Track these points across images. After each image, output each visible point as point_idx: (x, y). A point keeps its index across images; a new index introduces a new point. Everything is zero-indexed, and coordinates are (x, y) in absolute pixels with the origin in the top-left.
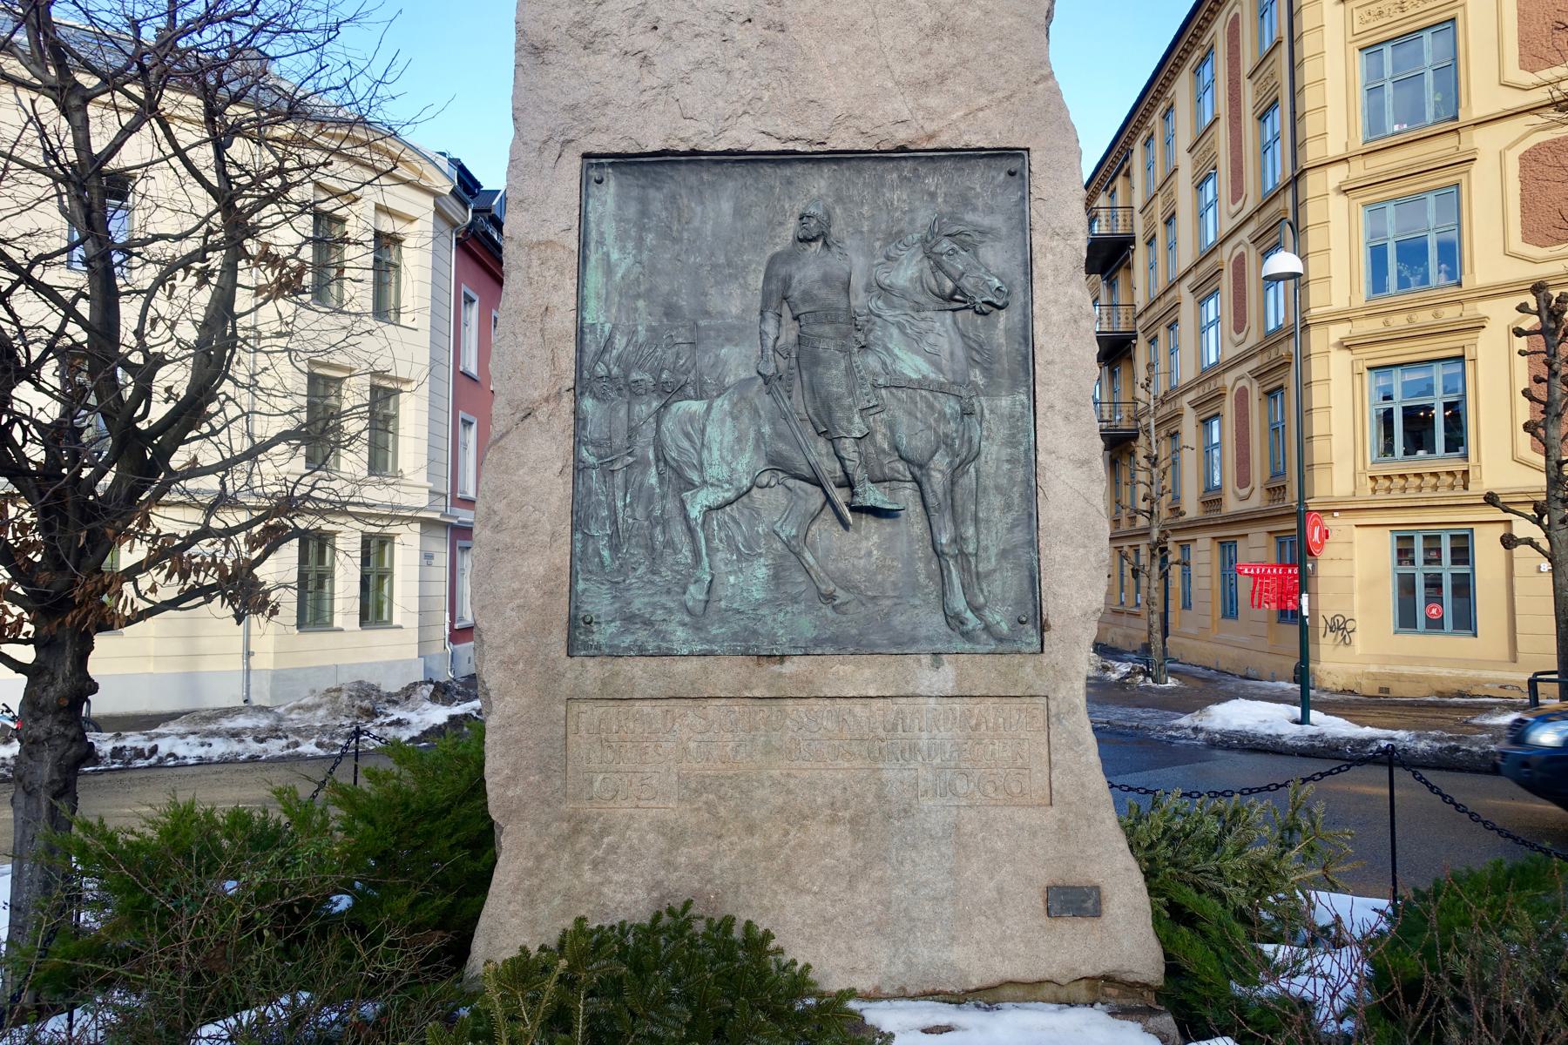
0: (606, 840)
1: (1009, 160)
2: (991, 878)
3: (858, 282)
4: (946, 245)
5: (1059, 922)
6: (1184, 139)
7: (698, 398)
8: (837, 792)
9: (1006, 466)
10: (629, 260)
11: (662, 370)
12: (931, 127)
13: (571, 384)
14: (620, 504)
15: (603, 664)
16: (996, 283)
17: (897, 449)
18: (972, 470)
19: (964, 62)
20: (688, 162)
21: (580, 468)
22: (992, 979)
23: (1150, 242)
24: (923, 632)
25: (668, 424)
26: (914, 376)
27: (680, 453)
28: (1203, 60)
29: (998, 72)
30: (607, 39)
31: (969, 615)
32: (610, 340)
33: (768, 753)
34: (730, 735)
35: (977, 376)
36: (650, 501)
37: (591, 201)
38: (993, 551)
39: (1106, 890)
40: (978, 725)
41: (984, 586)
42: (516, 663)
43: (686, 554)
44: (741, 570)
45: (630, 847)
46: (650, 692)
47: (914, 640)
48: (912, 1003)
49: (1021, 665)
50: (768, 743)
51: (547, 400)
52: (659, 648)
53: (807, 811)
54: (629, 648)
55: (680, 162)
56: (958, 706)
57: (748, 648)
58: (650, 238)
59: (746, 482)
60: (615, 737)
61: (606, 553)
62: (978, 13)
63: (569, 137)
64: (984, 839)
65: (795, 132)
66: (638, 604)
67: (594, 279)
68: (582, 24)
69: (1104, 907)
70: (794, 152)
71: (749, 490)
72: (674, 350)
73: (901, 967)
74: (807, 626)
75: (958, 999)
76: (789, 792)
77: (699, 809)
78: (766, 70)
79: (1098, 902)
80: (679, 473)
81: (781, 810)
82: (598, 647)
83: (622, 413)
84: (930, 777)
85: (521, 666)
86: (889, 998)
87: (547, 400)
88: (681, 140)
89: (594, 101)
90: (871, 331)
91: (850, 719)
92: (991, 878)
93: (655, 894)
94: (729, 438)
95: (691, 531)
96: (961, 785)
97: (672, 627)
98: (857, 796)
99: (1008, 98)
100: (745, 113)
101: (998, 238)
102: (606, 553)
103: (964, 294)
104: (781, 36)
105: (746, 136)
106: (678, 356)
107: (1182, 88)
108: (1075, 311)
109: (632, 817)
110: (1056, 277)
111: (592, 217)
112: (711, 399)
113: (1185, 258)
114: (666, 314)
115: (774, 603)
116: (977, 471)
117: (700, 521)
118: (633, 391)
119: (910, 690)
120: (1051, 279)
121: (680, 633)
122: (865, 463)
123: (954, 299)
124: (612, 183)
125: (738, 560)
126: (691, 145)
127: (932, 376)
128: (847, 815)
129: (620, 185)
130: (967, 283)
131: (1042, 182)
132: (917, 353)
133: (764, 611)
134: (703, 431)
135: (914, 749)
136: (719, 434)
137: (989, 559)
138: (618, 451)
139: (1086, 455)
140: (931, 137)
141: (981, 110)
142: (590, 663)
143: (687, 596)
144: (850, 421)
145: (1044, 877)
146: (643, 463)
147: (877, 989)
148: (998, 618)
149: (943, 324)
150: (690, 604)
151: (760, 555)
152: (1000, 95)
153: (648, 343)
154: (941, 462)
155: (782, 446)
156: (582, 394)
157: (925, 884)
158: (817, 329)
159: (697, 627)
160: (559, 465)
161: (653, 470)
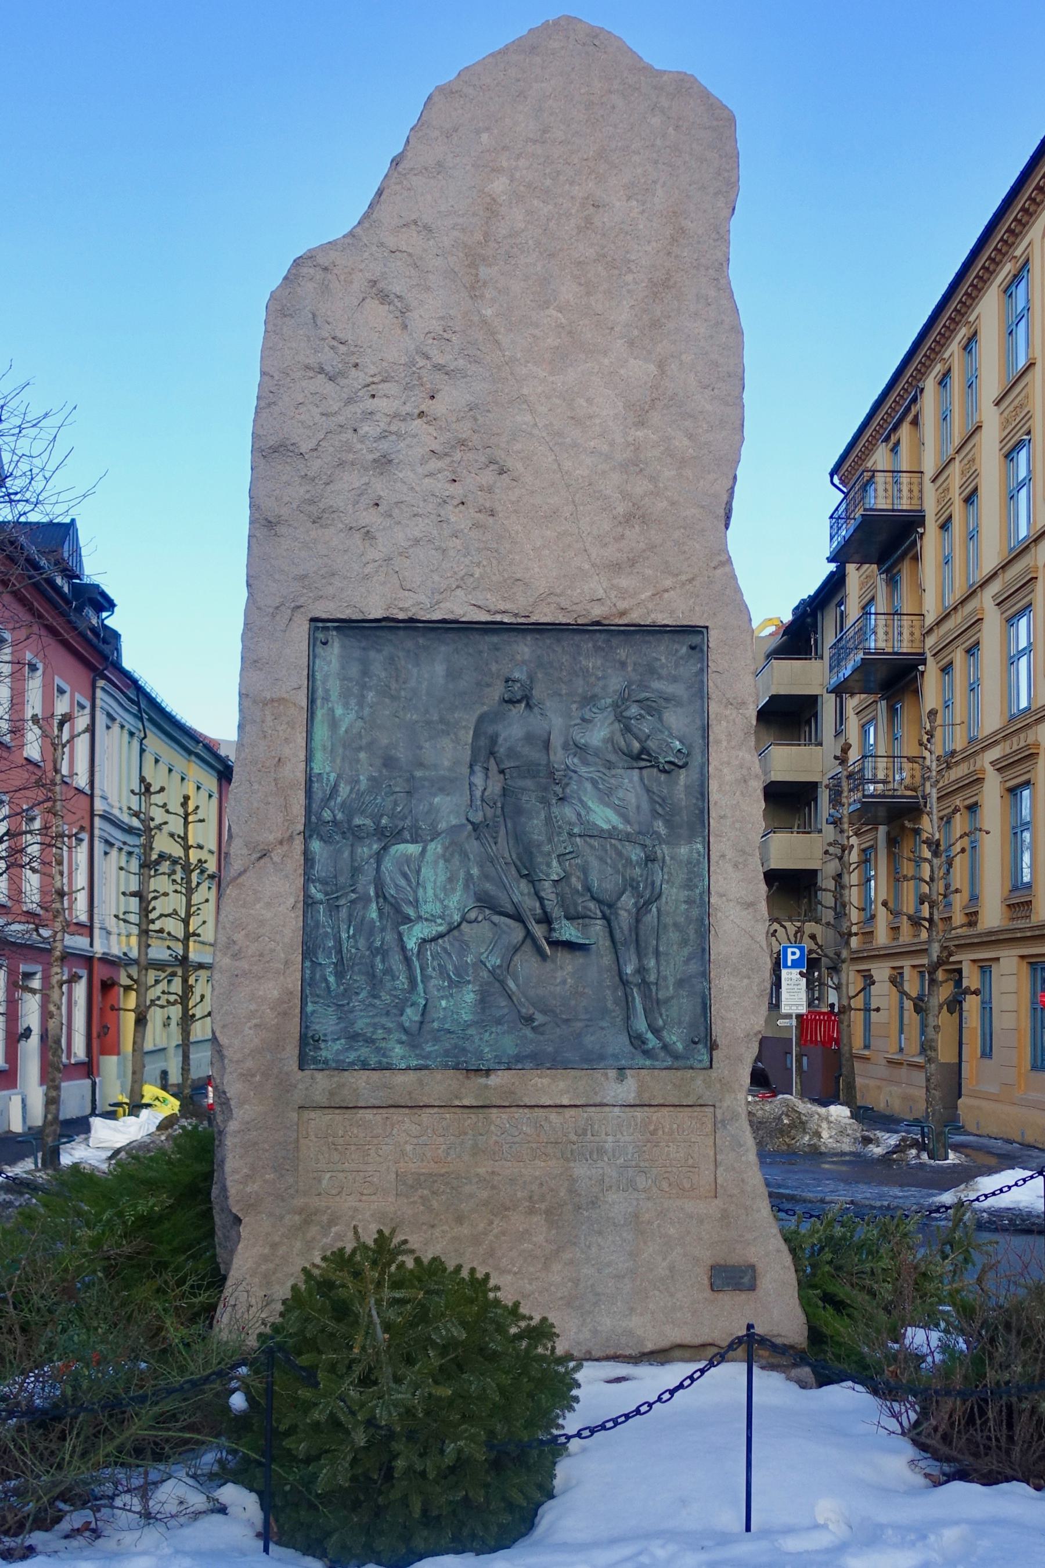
0: (333, 1230)
1: (691, 636)
2: (664, 1259)
3: (557, 741)
4: (634, 710)
6: (990, 386)
7: (414, 841)
8: (535, 1187)
9: (684, 906)
10: (352, 716)
11: (382, 816)
12: (622, 605)
14: (344, 936)
16: (677, 745)
18: (654, 909)
19: (652, 547)
20: (405, 628)
21: (309, 903)
23: (945, 526)
25: (387, 864)
26: (605, 826)
28: (1016, 278)
30: (335, 516)
31: (650, 1035)
33: (474, 1154)
35: (660, 827)
38: (671, 981)
39: (760, 1267)
40: (656, 1130)
41: (663, 1011)
42: (253, 1076)
43: (402, 981)
44: (451, 995)
46: (373, 1102)
47: (602, 1057)
49: (693, 1079)
51: (281, 843)
52: (380, 1062)
54: (353, 1063)
56: (639, 1114)
58: (371, 696)
60: (341, 1141)
61: (332, 979)
64: (659, 1226)
65: (502, 606)
66: (360, 1025)
68: (312, 502)
70: (502, 623)
71: (459, 925)
72: (392, 798)
73: (588, 1335)
74: (509, 1045)
77: (414, 1203)
79: (754, 1278)
80: (398, 910)
87: (281, 843)
88: (401, 609)
90: (568, 784)
91: (546, 1126)
94: (442, 878)
95: (407, 961)
98: (552, 1190)
100: (458, 587)
102: (332, 979)
105: (460, 607)
107: (989, 309)
108: (745, 772)
113: (990, 559)
114: (385, 765)
116: (659, 910)
117: (415, 951)
118: (356, 835)
120: (724, 744)
121: (399, 1050)
122: (562, 903)
123: (641, 757)
125: (450, 987)
126: (410, 614)
127: (621, 826)
128: (543, 1207)
129: (343, 647)
131: (718, 657)
132: (607, 805)
135: (601, 1151)
136: (433, 875)
137: (668, 988)
139: (751, 899)
140: (622, 614)
142: (319, 1076)
148: (674, 1038)
149: (631, 781)
150: (407, 1024)
152: (684, 578)
154: (627, 901)
156: (311, 836)
157: (609, 1264)
158: (521, 783)
161: (374, 906)
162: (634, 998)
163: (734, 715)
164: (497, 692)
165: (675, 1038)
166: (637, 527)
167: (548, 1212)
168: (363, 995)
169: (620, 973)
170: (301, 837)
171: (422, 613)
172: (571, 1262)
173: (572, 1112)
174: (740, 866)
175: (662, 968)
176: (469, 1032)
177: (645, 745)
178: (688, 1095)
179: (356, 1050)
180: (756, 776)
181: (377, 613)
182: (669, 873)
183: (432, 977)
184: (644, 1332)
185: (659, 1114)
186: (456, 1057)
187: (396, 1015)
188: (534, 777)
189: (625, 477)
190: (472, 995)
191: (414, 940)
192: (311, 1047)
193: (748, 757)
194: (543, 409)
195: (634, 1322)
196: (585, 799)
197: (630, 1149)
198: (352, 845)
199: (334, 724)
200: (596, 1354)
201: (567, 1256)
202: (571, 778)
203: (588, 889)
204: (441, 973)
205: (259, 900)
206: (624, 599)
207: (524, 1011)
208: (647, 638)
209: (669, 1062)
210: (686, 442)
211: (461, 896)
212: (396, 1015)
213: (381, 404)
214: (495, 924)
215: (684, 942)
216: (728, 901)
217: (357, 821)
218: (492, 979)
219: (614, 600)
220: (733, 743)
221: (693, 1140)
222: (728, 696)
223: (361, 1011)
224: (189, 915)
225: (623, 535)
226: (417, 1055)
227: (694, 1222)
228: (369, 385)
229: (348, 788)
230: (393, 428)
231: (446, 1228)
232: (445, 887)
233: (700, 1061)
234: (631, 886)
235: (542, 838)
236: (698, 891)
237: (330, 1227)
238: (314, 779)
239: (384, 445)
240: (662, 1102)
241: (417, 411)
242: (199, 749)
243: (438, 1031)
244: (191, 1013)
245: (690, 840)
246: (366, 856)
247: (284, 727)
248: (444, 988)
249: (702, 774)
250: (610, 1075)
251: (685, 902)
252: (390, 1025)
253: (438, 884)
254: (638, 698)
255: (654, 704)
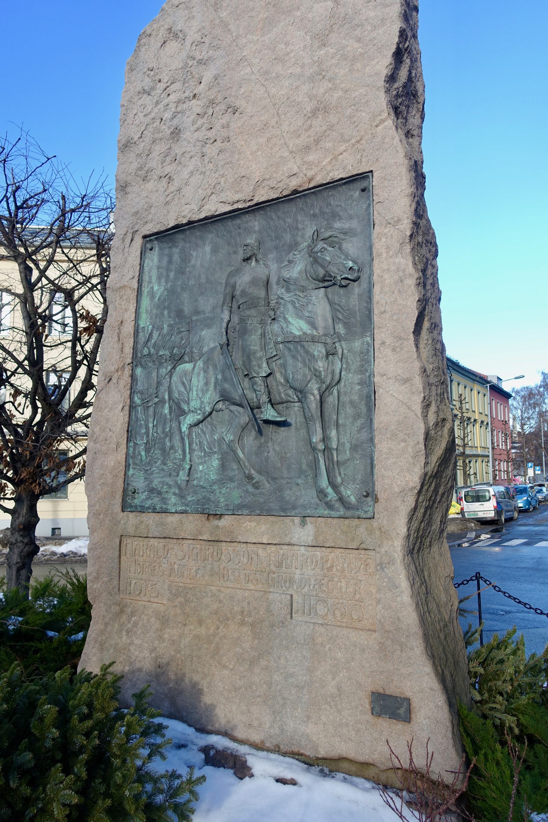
0: (133, 619)
2: (333, 679)
4: (321, 245)
5: (380, 721)
8: (245, 604)
9: (358, 387)
10: (162, 289)
11: (174, 348)
12: (310, 174)
13: (129, 361)
14: (151, 425)
15: (137, 516)
16: (350, 264)
17: (288, 382)
18: (335, 392)
19: (331, 127)
20: (189, 228)
21: (132, 407)
22: (334, 753)
24: (301, 501)
26: (297, 333)
27: (179, 394)
29: (352, 126)
30: (152, 173)
31: (330, 490)
32: (151, 335)
33: (212, 575)
34: (193, 562)
35: (341, 329)
36: (165, 424)
37: (146, 261)
38: (348, 445)
39: (415, 703)
40: (332, 567)
41: (342, 470)
42: (100, 514)
43: (179, 454)
44: (205, 462)
45: (143, 625)
46: (157, 534)
47: (294, 507)
48: (281, 758)
49: (357, 527)
50: (212, 569)
52: (161, 508)
53: (229, 615)
54: (149, 508)
55: (185, 230)
56: (318, 553)
57: (204, 510)
58: (172, 274)
59: (208, 409)
60: (141, 559)
61: (143, 453)
62: (340, 93)
63: (136, 229)
64: (330, 649)
66: (156, 483)
67: (145, 302)
69: (413, 715)
71: (210, 414)
72: (180, 336)
73: (277, 731)
74: (236, 496)
75: (310, 762)
76: (220, 602)
77: (176, 606)
78: (223, 166)
79: (409, 711)
80: (179, 407)
81: (216, 613)
82: (136, 507)
83: (154, 374)
84: (300, 601)
85: (102, 516)
86: (269, 750)
87: (117, 371)
89: (145, 207)
91: (255, 557)
92: (333, 679)
93: (153, 655)
94: (202, 383)
96: (321, 609)
97: (170, 495)
98: (255, 609)
99: (358, 142)
100: (212, 193)
101: (355, 235)
102: (143, 453)
103: (330, 276)
104: (228, 144)
105: (215, 207)
106: (182, 339)
108: (401, 274)
109: (145, 607)
110: (387, 252)
111: (146, 269)
112: (196, 362)
114: (178, 316)
115: (221, 482)
116: (339, 392)
118: (159, 361)
119: (287, 540)
120: (384, 255)
121: (173, 499)
123: (327, 281)
124: (157, 249)
125: (205, 456)
127: (309, 332)
128: (250, 620)
129: (161, 249)
130: (334, 270)
132: (301, 318)
133: (215, 487)
134: (191, 380)
135: (291, 581)
136: (197, 382)
137: (345, 452)
138: (151, 396)
139: (407, 375)
140: (310, 181)
141: (341, 154)
142: (131, 515)
143: (179, 478)
144: (260, 367)
145: (370, 685)
146: (163, 402)
147: (263, 742)
148: (349, 493)
151: (215, 452)
152: (353, 141)
153: (168, 334)
154: (314, 387)
155: (226, 386)
156: (136, 366)
157: (292, 675)
158: (248, 312)
159: (182, 496)
160: (121, 406)
161: (167, 405)
162: (319, 461)
163: (392, 232)
164: (241, 255)
165: (350, 493)
166: (320, 116)
167: (252, 625)
168: (159, 462)
169: (310, 442)
170: (130, 367)
171: (194, 216)
172: (266, 668)
173: (273, 548)
174: (398, 350)
175: (341, 437)
176: (214, 487)
177: (328, 269)
178: (353, 539)
179: (152, 499)
180: (410, 275)
181: (172, 224)
182: (347, 363)
183: (195, 450)
184: (318, 739)
185: (333, 555)
186: (203, 505)
187: (174, 476)
188: (256, 307)
189: (312, 85)
190: (217, 462)
191: (186, 425)
192: (130, 497)
193: (403, 261)
194: (255, 61)
195: (310, 729)
196: (287, 316)
197: (313, 582)
198: (158, 368)
199: (152, 295)
200: (283, 748)
201: (263, 663)
202: (280, 304)
203: (287, 381)
204: (200, 447)
205: (106, 407)
206: (312, 169)
207: (247, 472)
208: (330, 193)
209: (342, 512)
210: (356, 45)
211: (211, 394)
212: (174, 476)
213: (173, 97)
214: (231, 411)
215: (356, 417)
216: (388, 379)
217: (161, 353)
218: (228, 450)
219: (305, 172)
220: (391, 253)
221: (359, 578)
222: (386, 218)
223: (157, 473)
224: (464, 437)
225: (311, 126)
226: (182, 503)
227: (358, 650)
228: (166, 89)
229: (158, 333)
230: (179, 109)
231: (192, 627)
232: (202, 389)
233: (366, 512)
234: (315, 375)
235: (257, 348)
236: (368, 374)
237: (132, 616)
238: (140, 331)
239: (175, 122)
240: (333, 545)
241: (192, 95)
242: (477, 379)
243: (197, 486)
244: (468, 472)
245: (362, 335)
246: (164, 374)
247: (125, 302)
248: (201, 457)
249: (370, 283)
250: (296, 521)
251: (358, 384)
252: (171, 483)
253: (199, 387)
254: (323, 238)
255: (336, 239)
